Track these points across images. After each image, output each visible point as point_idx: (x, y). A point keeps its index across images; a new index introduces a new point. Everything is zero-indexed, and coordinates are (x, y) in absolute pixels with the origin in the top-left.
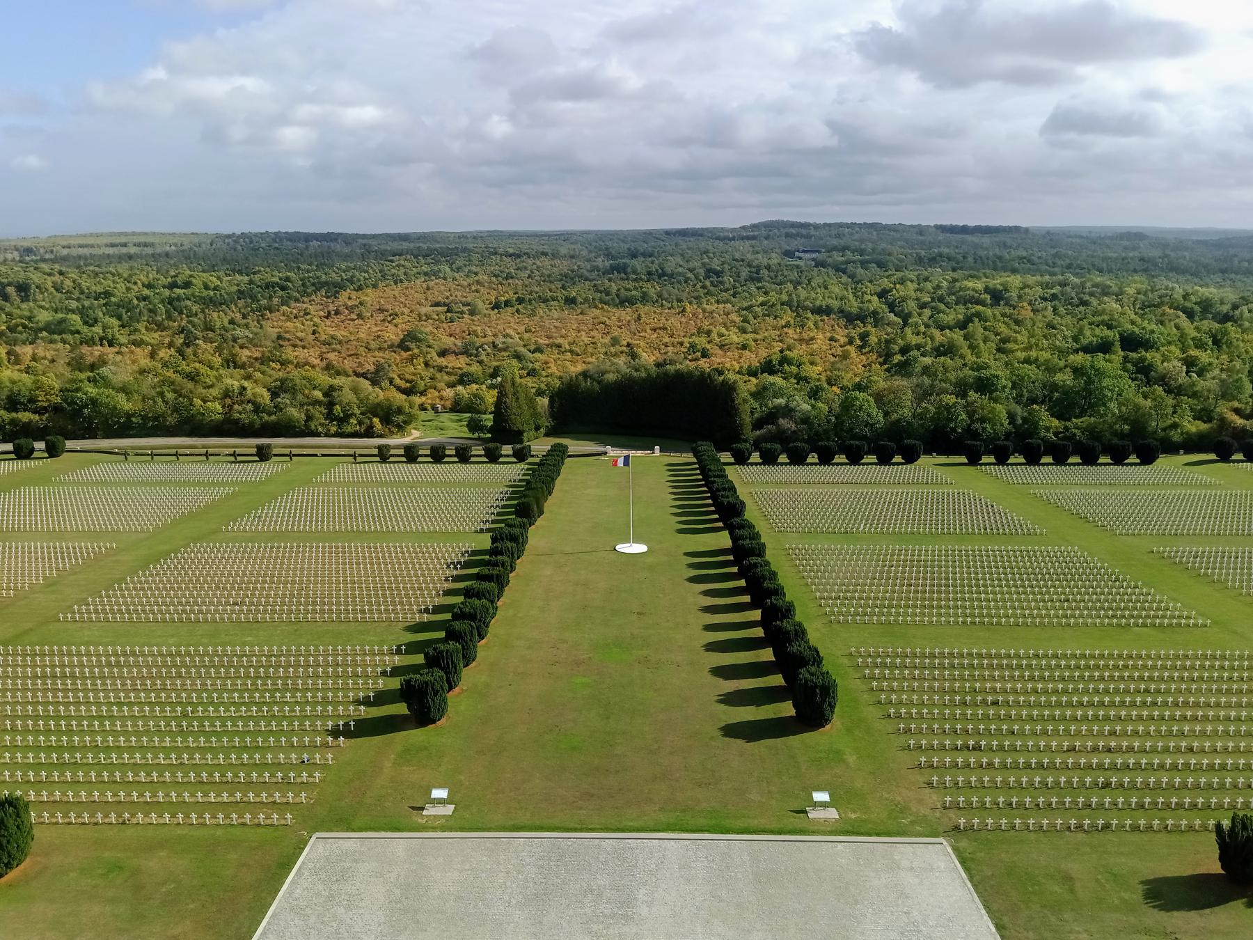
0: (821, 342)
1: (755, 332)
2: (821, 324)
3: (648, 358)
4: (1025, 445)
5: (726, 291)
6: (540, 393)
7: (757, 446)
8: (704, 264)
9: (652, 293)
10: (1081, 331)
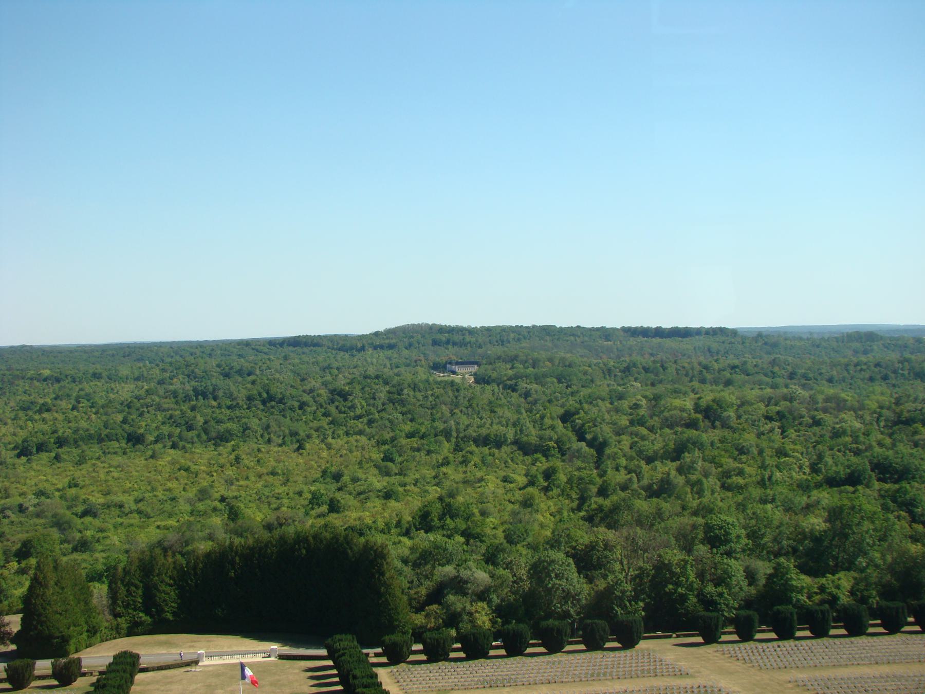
0: (492, 485)
1: (401, 473)
2: (490, 459)
3: (256, 515)
4: (772, 615)
5: (358, 417)
6: (95, 577)
7: (418, 636)
8: (325, 384)
9: (254, 423)
10: (820, 457)
